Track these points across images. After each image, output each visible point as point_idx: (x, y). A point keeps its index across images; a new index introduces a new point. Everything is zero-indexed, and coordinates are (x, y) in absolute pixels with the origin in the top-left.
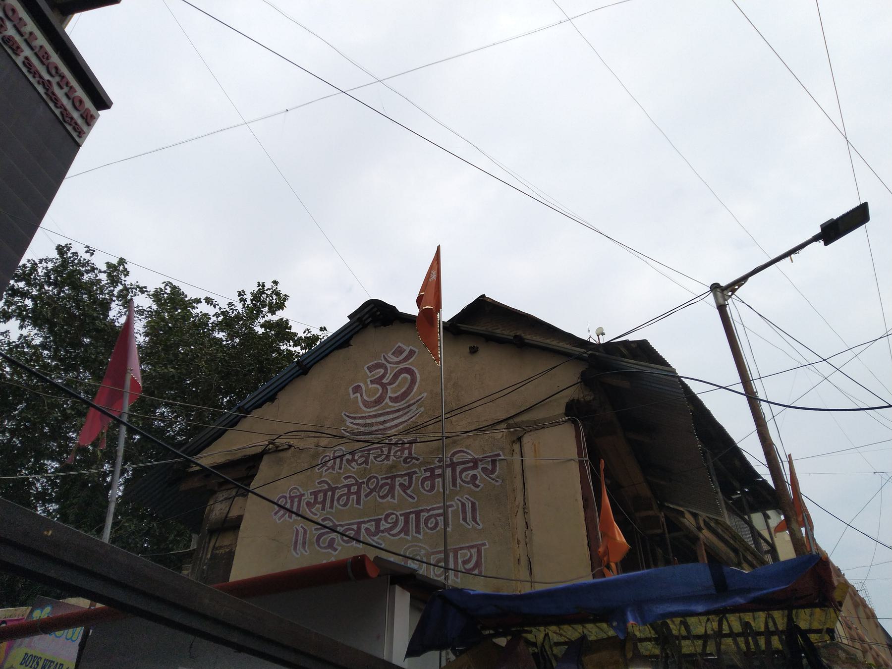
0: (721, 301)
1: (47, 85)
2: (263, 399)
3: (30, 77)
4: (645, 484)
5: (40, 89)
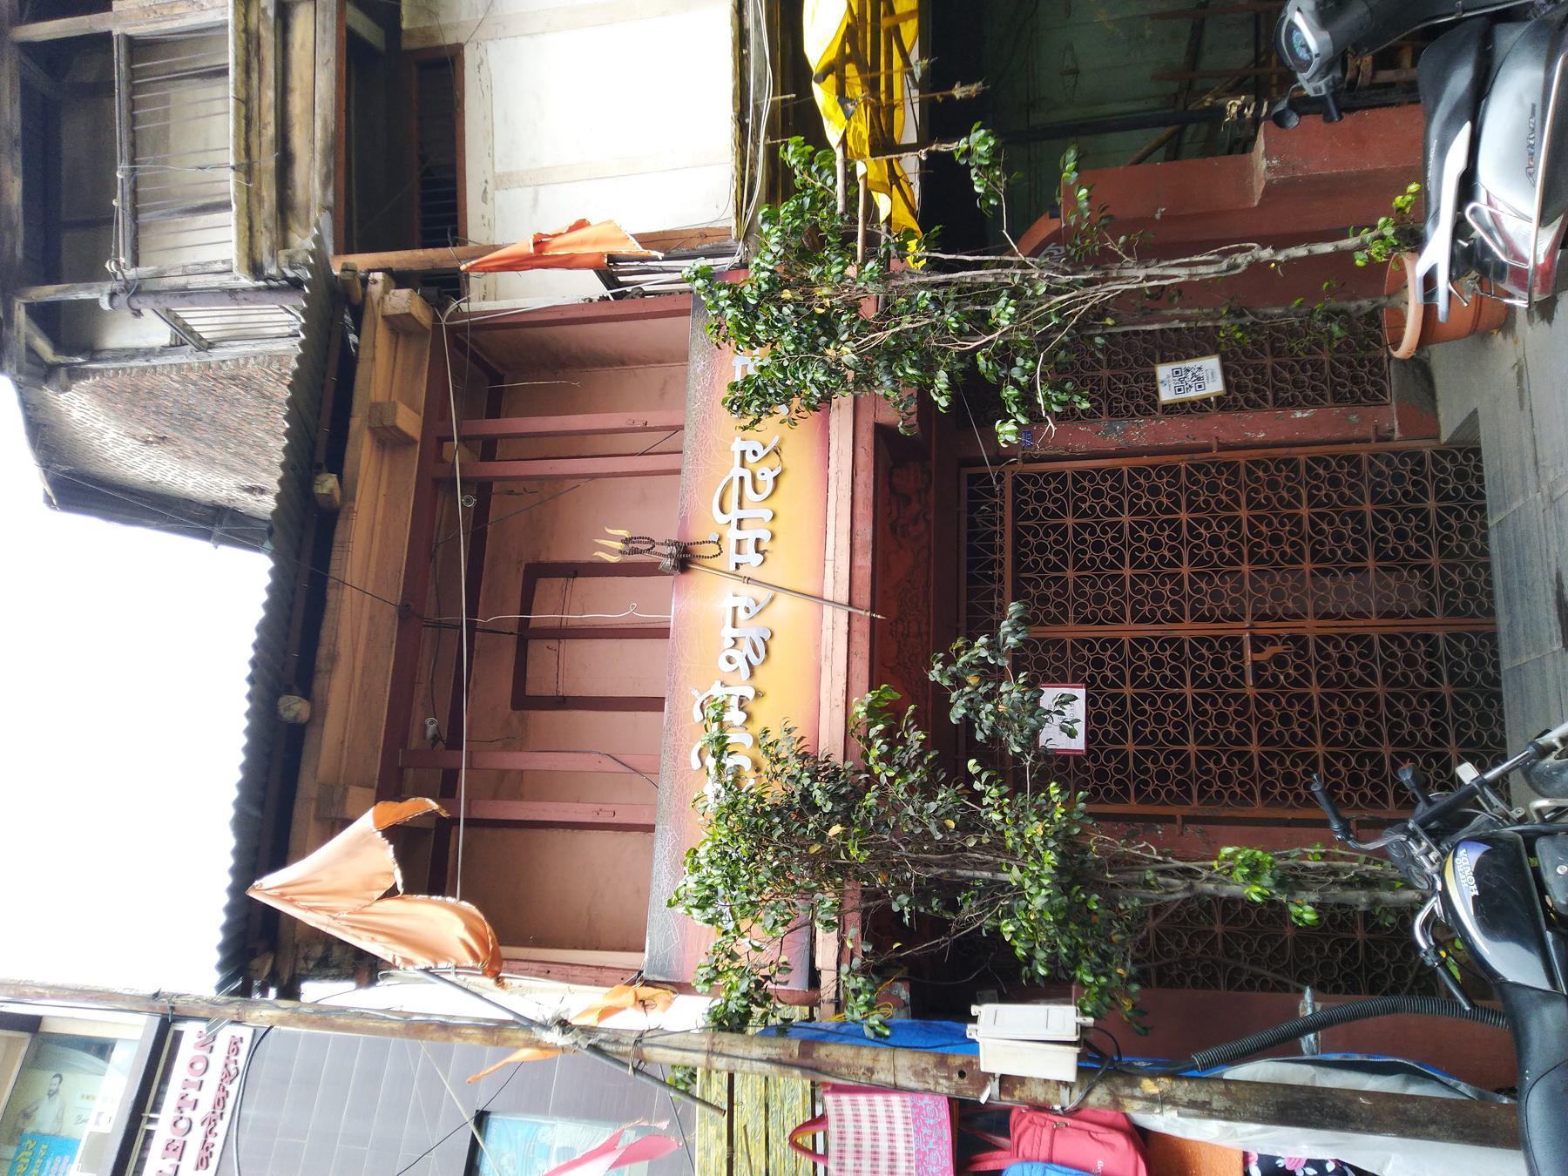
0: (520, 1043)
1: (210, 1123)
2: (355, 218)
3: (217, 1151)
4: (231, 175)
5: (221, 1127)
